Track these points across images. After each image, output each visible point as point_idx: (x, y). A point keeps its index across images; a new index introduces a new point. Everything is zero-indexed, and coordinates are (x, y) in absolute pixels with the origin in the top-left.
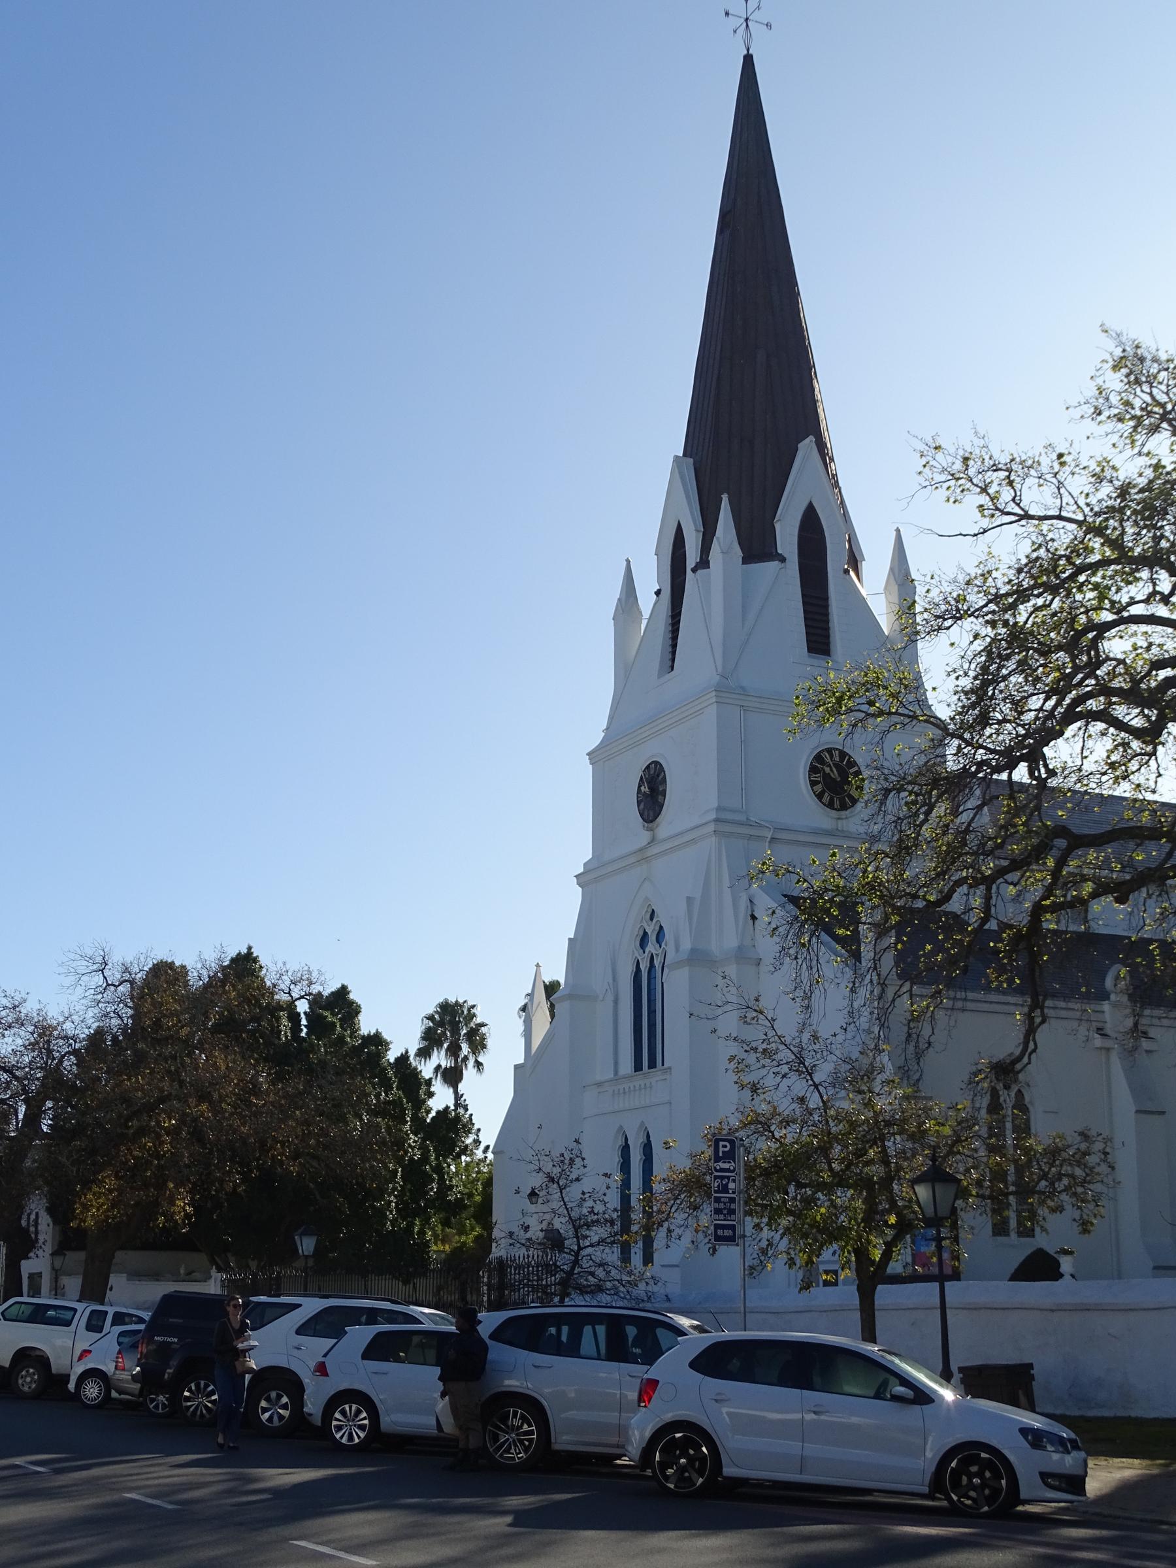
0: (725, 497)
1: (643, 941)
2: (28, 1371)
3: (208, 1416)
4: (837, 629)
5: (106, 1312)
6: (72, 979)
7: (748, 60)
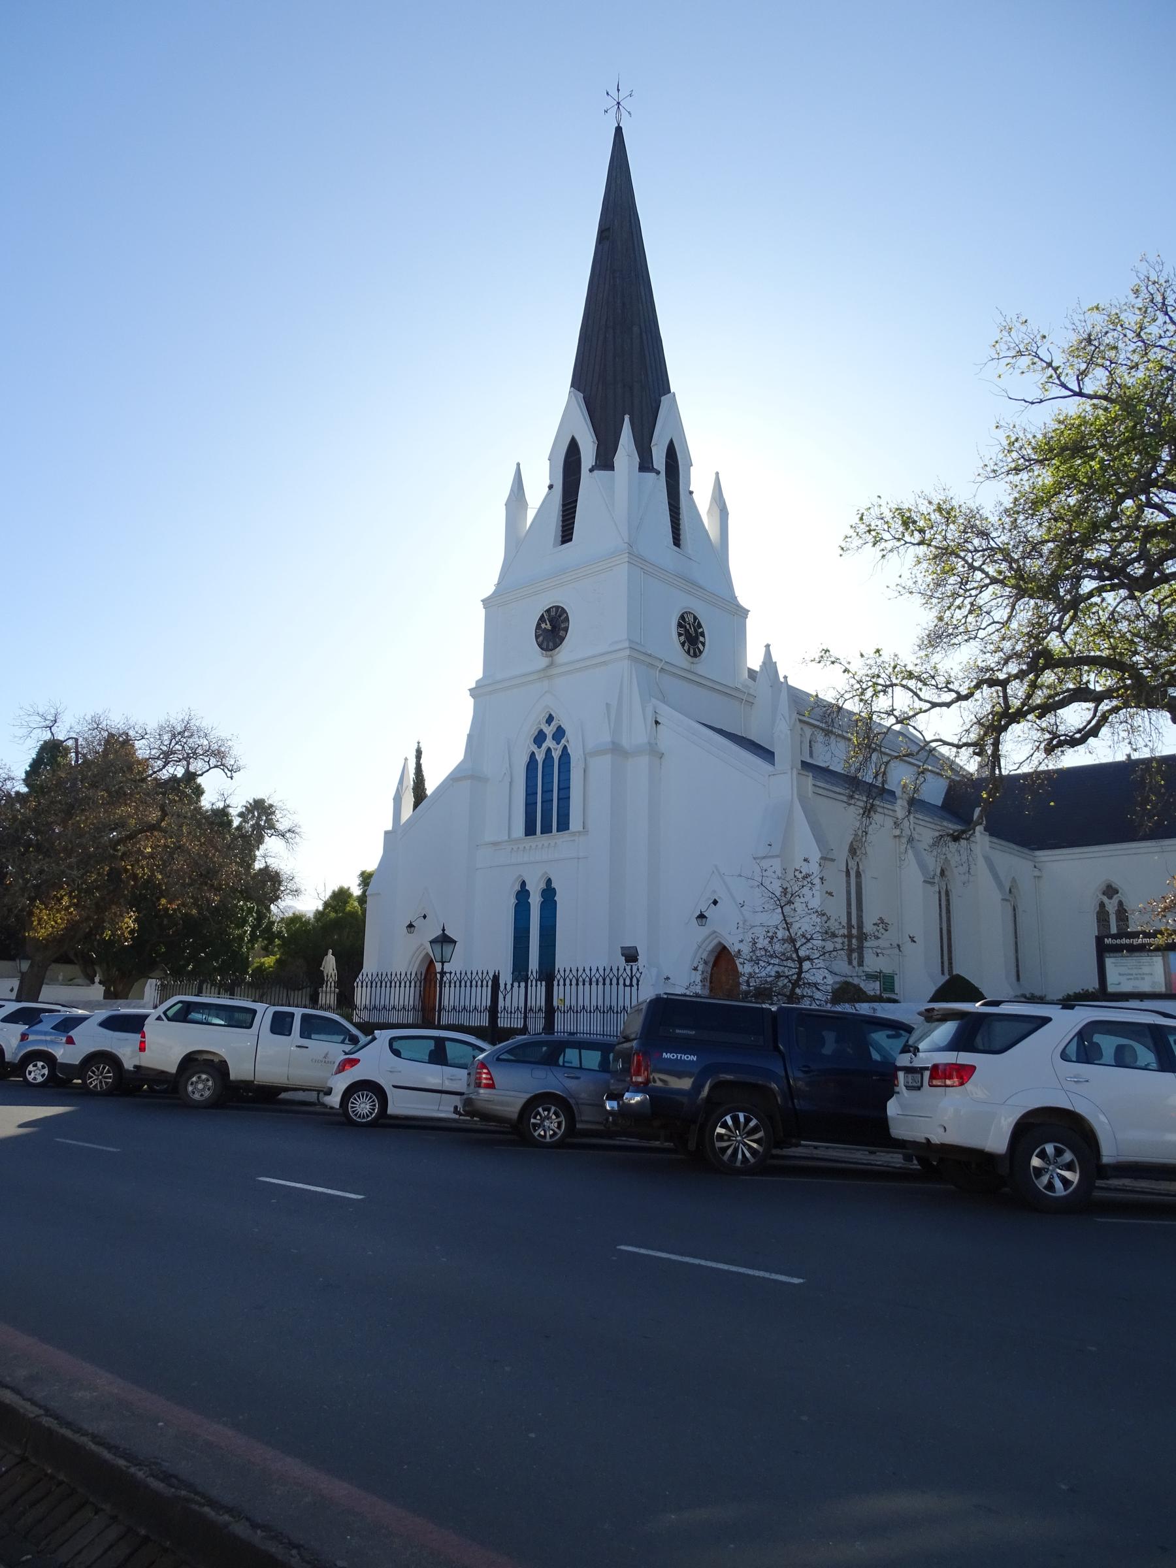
0: (627, 417)
1: (540, 738)
2: (199, 1077)
3: (752, 1160)
4: (687, 528)
5: (293, 1015)
6: (24, 731)
7: (619, 130)
